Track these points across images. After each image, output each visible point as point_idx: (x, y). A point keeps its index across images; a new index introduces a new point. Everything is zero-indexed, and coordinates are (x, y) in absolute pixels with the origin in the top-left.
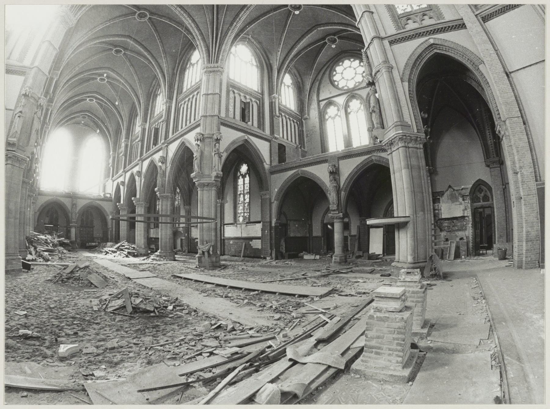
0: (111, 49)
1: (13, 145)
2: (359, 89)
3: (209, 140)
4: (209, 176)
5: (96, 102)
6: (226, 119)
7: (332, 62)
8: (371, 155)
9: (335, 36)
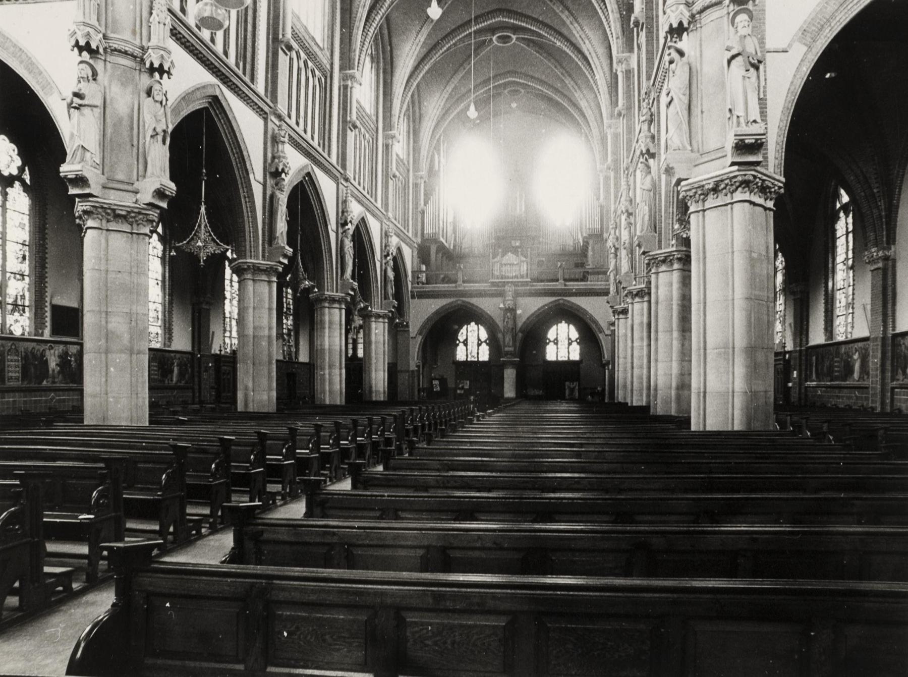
5: (517, 39)
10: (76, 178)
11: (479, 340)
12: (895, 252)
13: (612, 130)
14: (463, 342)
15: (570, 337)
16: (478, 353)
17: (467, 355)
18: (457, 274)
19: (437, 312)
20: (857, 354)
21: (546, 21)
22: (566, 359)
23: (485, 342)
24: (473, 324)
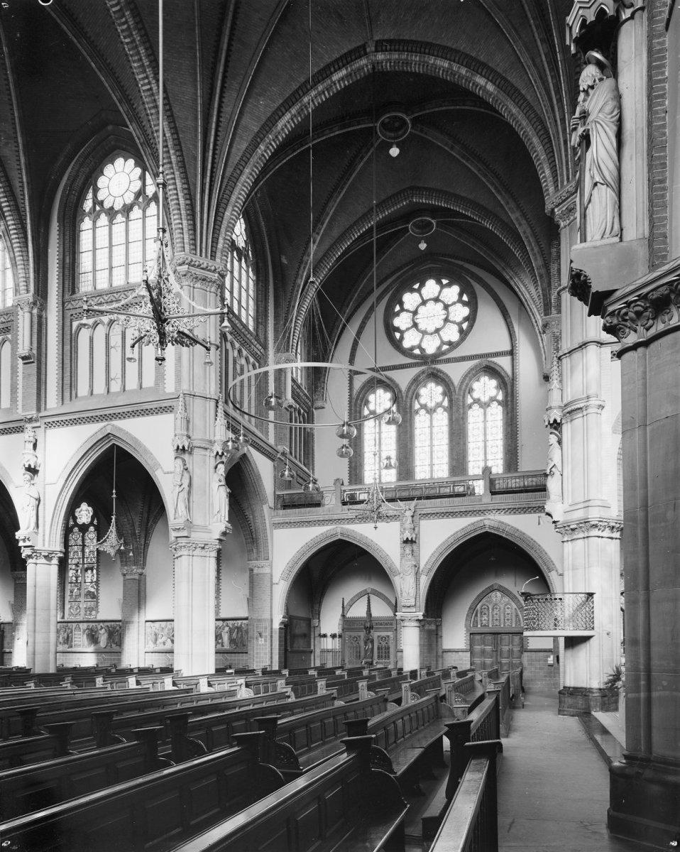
2: (448, 361)
3: (203, 452)
4: (205, 529)
7: (398, 278)
8: (482, 518)
9: (433, 219)
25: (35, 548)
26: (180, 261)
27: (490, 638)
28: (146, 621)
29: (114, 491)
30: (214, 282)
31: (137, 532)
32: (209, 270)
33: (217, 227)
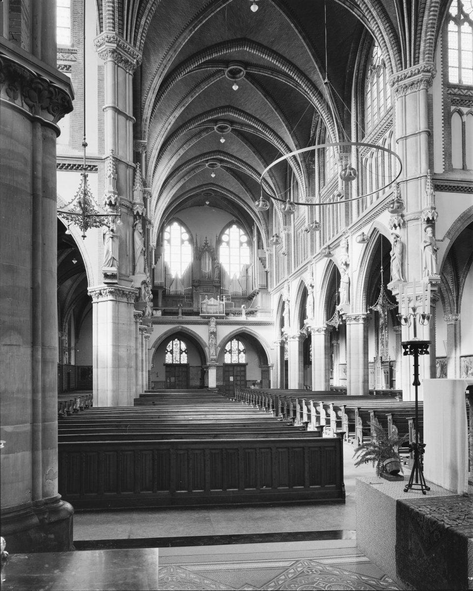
0: (220, 71)
1: (113, 276)
3: (415, 223)
5: (221, 166)
6: (447, 176)
10: (112, 275)
11: (181, 350)
12: (460, 317)
13: (286, 232)
14: (170, 352)
15: (240, 348)
16: (180, 359)
17: (173, 360)
18: (178, 310)
19: (165, 333)
20: (438, 364)
21: (247, 162)
22: (237, 362)
23: (185, 351)
24: (176, 340)
25: (347, 315)
26: (392, 83)
27: (102, 552)
28: (462, 357)
29: (382, 267)
30: (421, 80)
31: (451, 287)
32: (414, 75)
33: (137, 31)
